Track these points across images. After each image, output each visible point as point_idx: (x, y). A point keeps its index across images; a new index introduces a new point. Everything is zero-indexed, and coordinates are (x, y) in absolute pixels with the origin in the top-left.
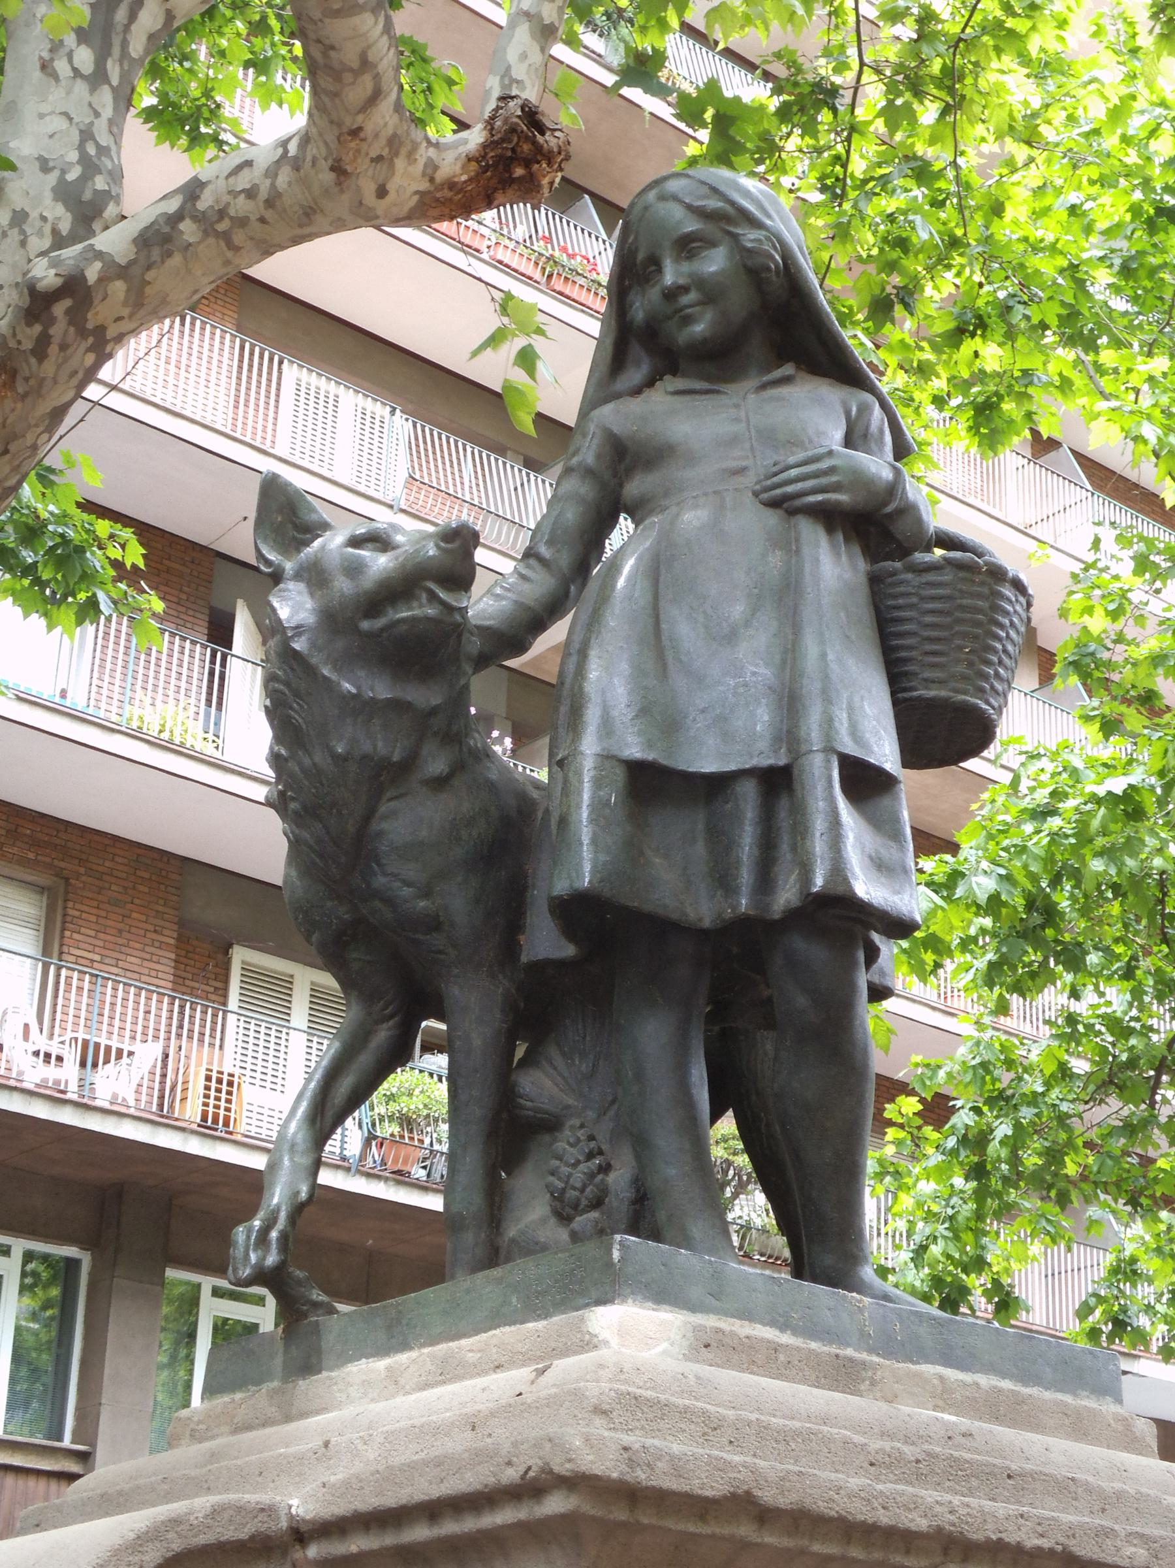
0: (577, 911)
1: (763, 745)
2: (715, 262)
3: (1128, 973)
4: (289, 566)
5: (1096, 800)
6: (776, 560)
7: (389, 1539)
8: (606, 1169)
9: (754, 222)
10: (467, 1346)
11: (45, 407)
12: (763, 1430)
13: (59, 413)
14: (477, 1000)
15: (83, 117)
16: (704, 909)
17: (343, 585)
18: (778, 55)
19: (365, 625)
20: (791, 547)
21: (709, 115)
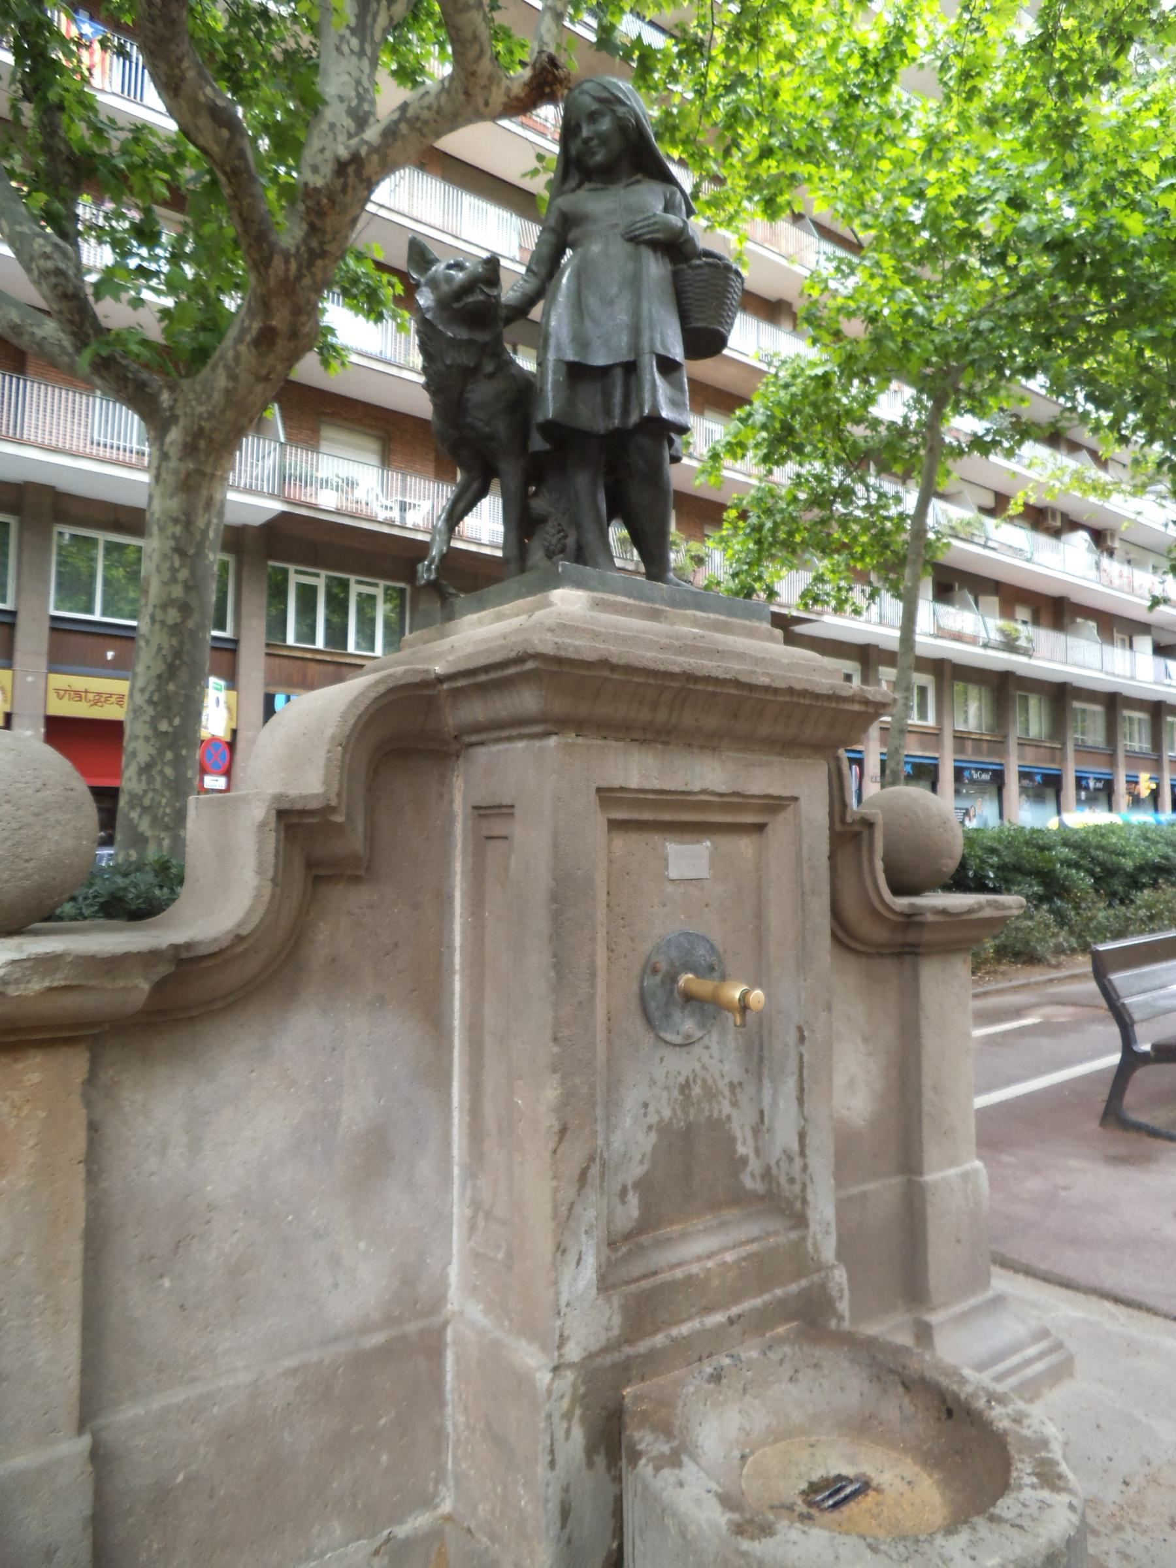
0: (550, 429)
1: (625, 351)
2: (605, 125)
3: (824, 455)
4: (422, 280)
5: (811, 378)
6: (630, 267)
7: (472, 681)
8: (566, 537)
9: (621, 102)
10: (506, 608)
11: (348, 218)
12: (616, 636)
13: (354, 221)
14: (511, 468)
15: (356, 73)
16: (600, 426)
17: (445, 288)
18: (676, 26)
19: (456, 306)
20: (637, 259)
21: (637, 54)
